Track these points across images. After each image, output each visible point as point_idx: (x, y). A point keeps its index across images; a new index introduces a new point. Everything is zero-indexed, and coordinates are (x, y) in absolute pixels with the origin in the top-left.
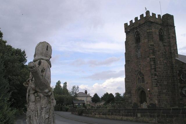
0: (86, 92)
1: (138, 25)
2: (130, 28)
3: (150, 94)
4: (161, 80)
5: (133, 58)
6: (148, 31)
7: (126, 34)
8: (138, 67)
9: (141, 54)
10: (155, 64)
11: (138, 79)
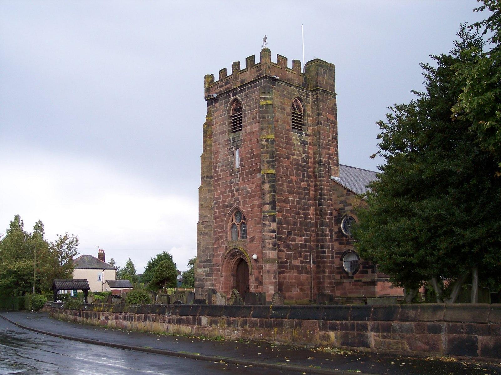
0: (102, 256)
1: (239, 84)
2: (218, 91)
3: (258, 268)
5: (222, 171)
6: (262, 103)
8: (233, 196)
10: (274, 192)
11: (231, 228)
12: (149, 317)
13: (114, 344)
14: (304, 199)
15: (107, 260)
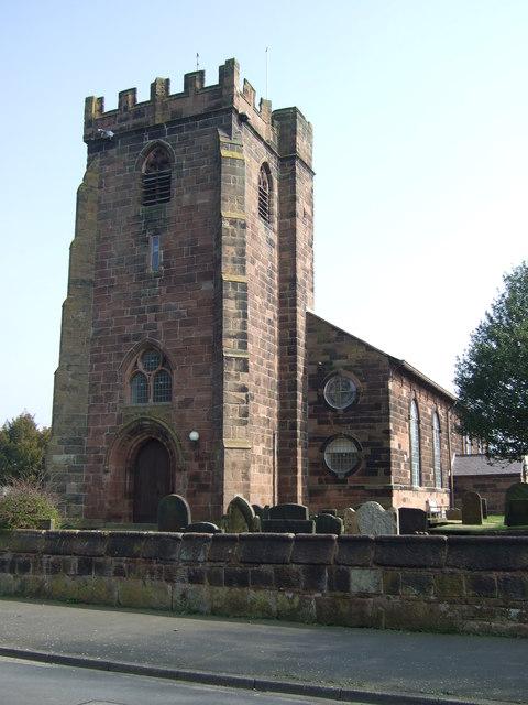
1: (169, 118)
2: (117, 127)
7: (89, 152)
9: (166, 255)
10: (245, 315)
13: (432, 698)
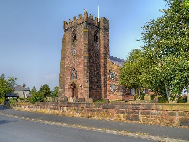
0: (24, 86)
4: (93, 77)
5: (69, 55)
9: (76, 51)
12: (42, 107)
14: (97, 65)
15: (26, 87)
